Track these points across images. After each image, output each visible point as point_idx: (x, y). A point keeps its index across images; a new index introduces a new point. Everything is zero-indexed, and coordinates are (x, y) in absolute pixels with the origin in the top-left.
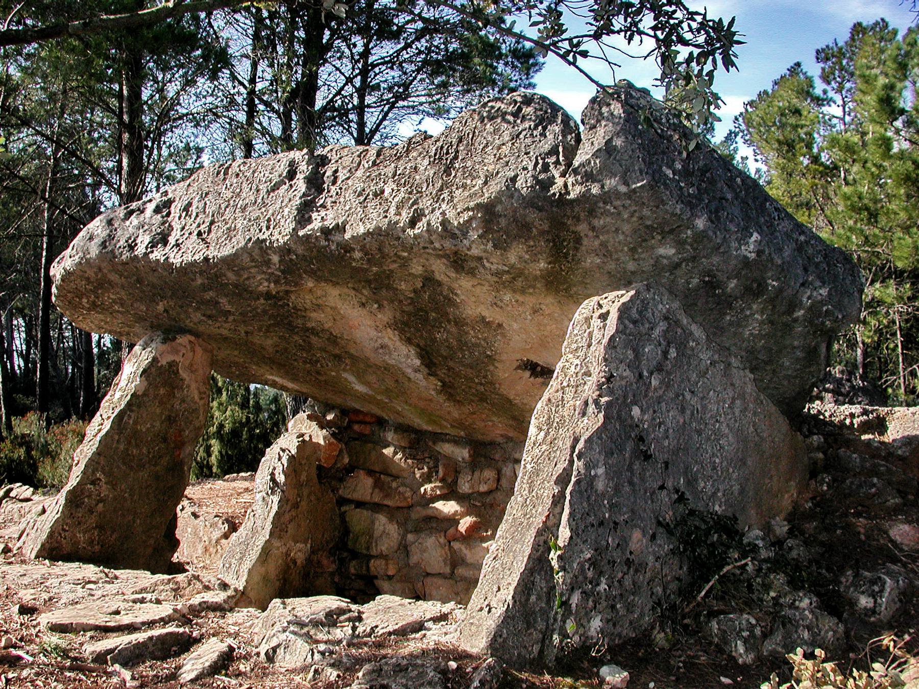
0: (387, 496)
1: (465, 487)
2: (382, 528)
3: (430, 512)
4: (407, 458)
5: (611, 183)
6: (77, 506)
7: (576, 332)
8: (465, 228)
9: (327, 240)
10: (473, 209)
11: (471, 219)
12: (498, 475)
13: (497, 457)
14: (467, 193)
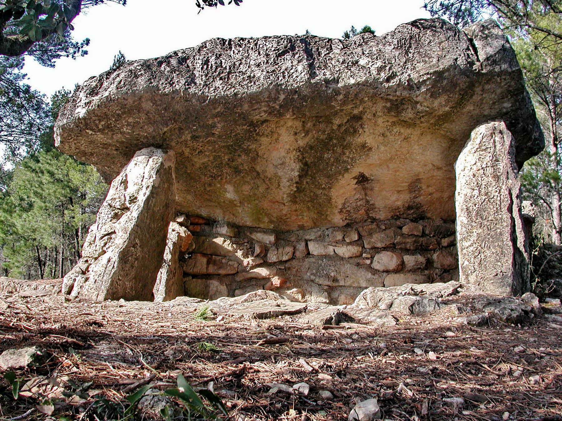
0: (220, 268)
1: (273, 257)
2: (215, 289)
3: (249, 276)
4: (233, 244)
5: (504, 66)
6: (126, 263)
7: (484, 140)
8: (419, 85)
9: (326, 87)
10: (431, 74)
11: (428, 79)
12: (294, 249)
13: (293, 239)
14: (428, 65)
